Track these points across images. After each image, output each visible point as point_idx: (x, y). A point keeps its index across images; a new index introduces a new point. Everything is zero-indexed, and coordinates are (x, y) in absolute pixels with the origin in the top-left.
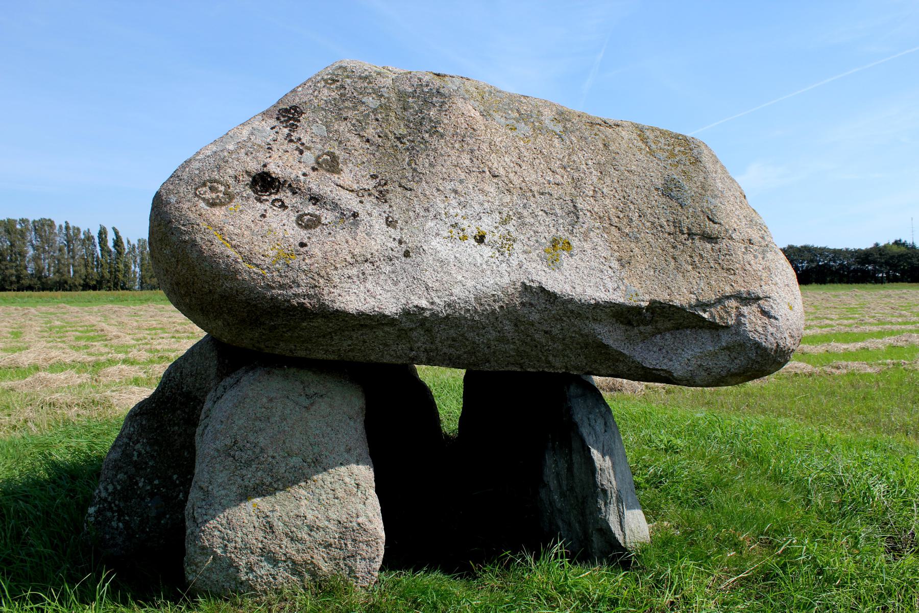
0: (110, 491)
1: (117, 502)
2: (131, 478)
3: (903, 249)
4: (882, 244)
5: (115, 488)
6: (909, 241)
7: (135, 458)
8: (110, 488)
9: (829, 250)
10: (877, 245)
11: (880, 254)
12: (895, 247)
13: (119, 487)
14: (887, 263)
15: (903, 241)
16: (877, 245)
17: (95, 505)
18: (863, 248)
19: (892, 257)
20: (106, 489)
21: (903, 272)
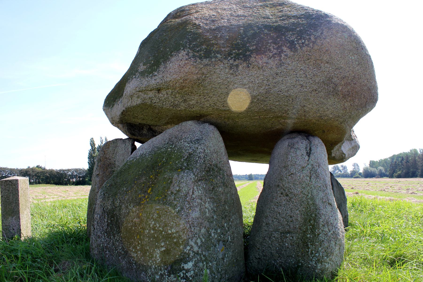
0: (199, 244)
1: (204, 253)
2: (208, 231)
3: (40, 170)
4: (31, 167)
5: (202, 241)
6: (43, 166)
7: (207, 215)
8: (199, 241)
9: (8, 169)
10: (29, 167)
11: (33, 171)
12: (37, 168)
13: (203, 240)
14: (36, 175)
15: (40, 166)
16: (29, 167)
17: (191, 260)
18: (48, 167)
19: (38, 173)
20: (196, 243)
21: (43, 180)
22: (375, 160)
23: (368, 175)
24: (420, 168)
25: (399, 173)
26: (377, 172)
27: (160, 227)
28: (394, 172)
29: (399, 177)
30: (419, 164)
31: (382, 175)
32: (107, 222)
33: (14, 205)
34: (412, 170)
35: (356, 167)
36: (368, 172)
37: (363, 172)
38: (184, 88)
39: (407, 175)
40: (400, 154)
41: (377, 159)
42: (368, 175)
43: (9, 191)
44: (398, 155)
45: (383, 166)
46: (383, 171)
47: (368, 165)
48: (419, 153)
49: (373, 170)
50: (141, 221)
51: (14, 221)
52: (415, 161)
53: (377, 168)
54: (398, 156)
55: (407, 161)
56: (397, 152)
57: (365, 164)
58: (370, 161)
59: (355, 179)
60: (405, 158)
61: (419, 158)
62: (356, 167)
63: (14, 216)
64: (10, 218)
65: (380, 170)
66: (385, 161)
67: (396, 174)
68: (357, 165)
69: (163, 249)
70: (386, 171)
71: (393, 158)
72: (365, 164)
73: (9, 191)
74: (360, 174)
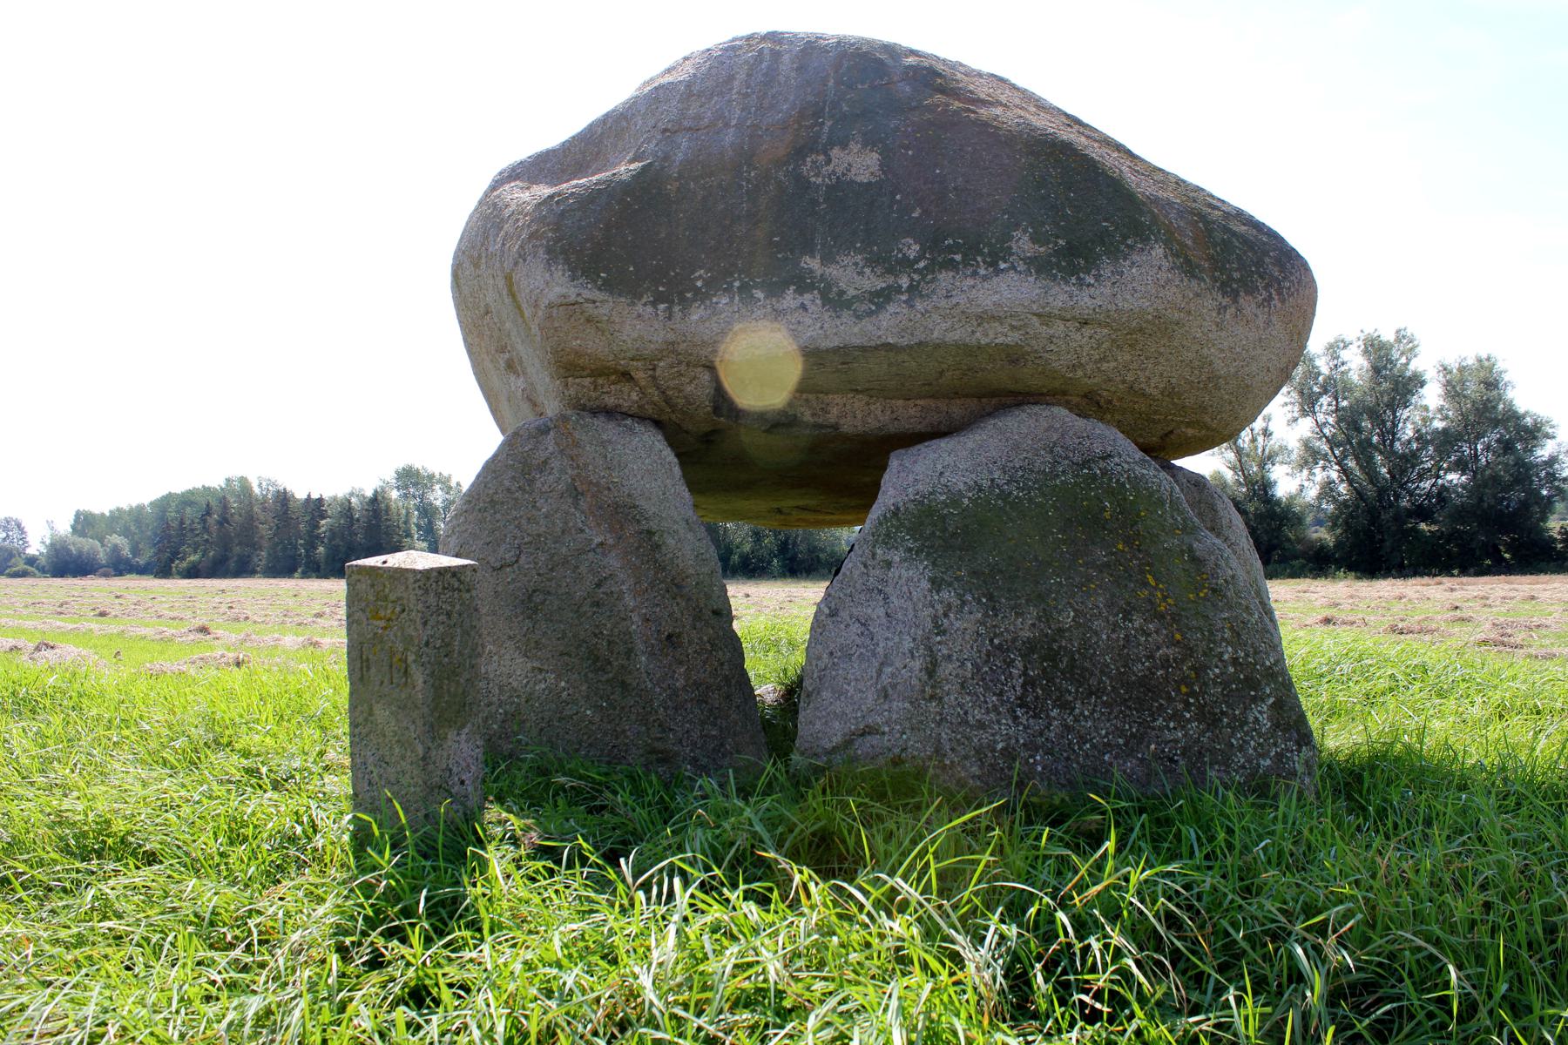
22: (96, 511)
23: (66, 563)
24: (265, 544)
25: (192, 558)
26: (102, 557)
27: (1247, 655)
28: (175, 555)
29: (193, 573)
30: (265, 530)
31: (120, 567)
32: (1025, 674)
33: (466, 675)
34: (237, 550)
35: (14, 534)
36: (68, 552)
37: (48, 556)
38: (1139, 333)
39: (217, 568)
40: (191, 492)
41: (102, 505)
42: (66, 563)
43: (449, 615)
44: (183, 494)
45: (126, 533)
46: (126, 552)
47: (64, 527)
48: (257, 490)
49: (87, 544)
50: (1190, 651)
51: (464, 746)
52: (251, 518)
53: (101, 541)
54: (187, 499)
55: (224, 521)
56: (180, 484)
57: (50, 524)
58: (78, 514)
59: (9, 581)
60: (214, 503)
61: (264, 509)
62: (14, 534)
63: (463, 726)
64: (451, 735)
65: (116, 549)
66: (137, 514)
67: (184, 565)
68: (19, 525)
69: (1272, 700)
70: (136, 551)
71: (164, 504)
72: (50, 524)
73: (449, 615)
74: (31, 561)
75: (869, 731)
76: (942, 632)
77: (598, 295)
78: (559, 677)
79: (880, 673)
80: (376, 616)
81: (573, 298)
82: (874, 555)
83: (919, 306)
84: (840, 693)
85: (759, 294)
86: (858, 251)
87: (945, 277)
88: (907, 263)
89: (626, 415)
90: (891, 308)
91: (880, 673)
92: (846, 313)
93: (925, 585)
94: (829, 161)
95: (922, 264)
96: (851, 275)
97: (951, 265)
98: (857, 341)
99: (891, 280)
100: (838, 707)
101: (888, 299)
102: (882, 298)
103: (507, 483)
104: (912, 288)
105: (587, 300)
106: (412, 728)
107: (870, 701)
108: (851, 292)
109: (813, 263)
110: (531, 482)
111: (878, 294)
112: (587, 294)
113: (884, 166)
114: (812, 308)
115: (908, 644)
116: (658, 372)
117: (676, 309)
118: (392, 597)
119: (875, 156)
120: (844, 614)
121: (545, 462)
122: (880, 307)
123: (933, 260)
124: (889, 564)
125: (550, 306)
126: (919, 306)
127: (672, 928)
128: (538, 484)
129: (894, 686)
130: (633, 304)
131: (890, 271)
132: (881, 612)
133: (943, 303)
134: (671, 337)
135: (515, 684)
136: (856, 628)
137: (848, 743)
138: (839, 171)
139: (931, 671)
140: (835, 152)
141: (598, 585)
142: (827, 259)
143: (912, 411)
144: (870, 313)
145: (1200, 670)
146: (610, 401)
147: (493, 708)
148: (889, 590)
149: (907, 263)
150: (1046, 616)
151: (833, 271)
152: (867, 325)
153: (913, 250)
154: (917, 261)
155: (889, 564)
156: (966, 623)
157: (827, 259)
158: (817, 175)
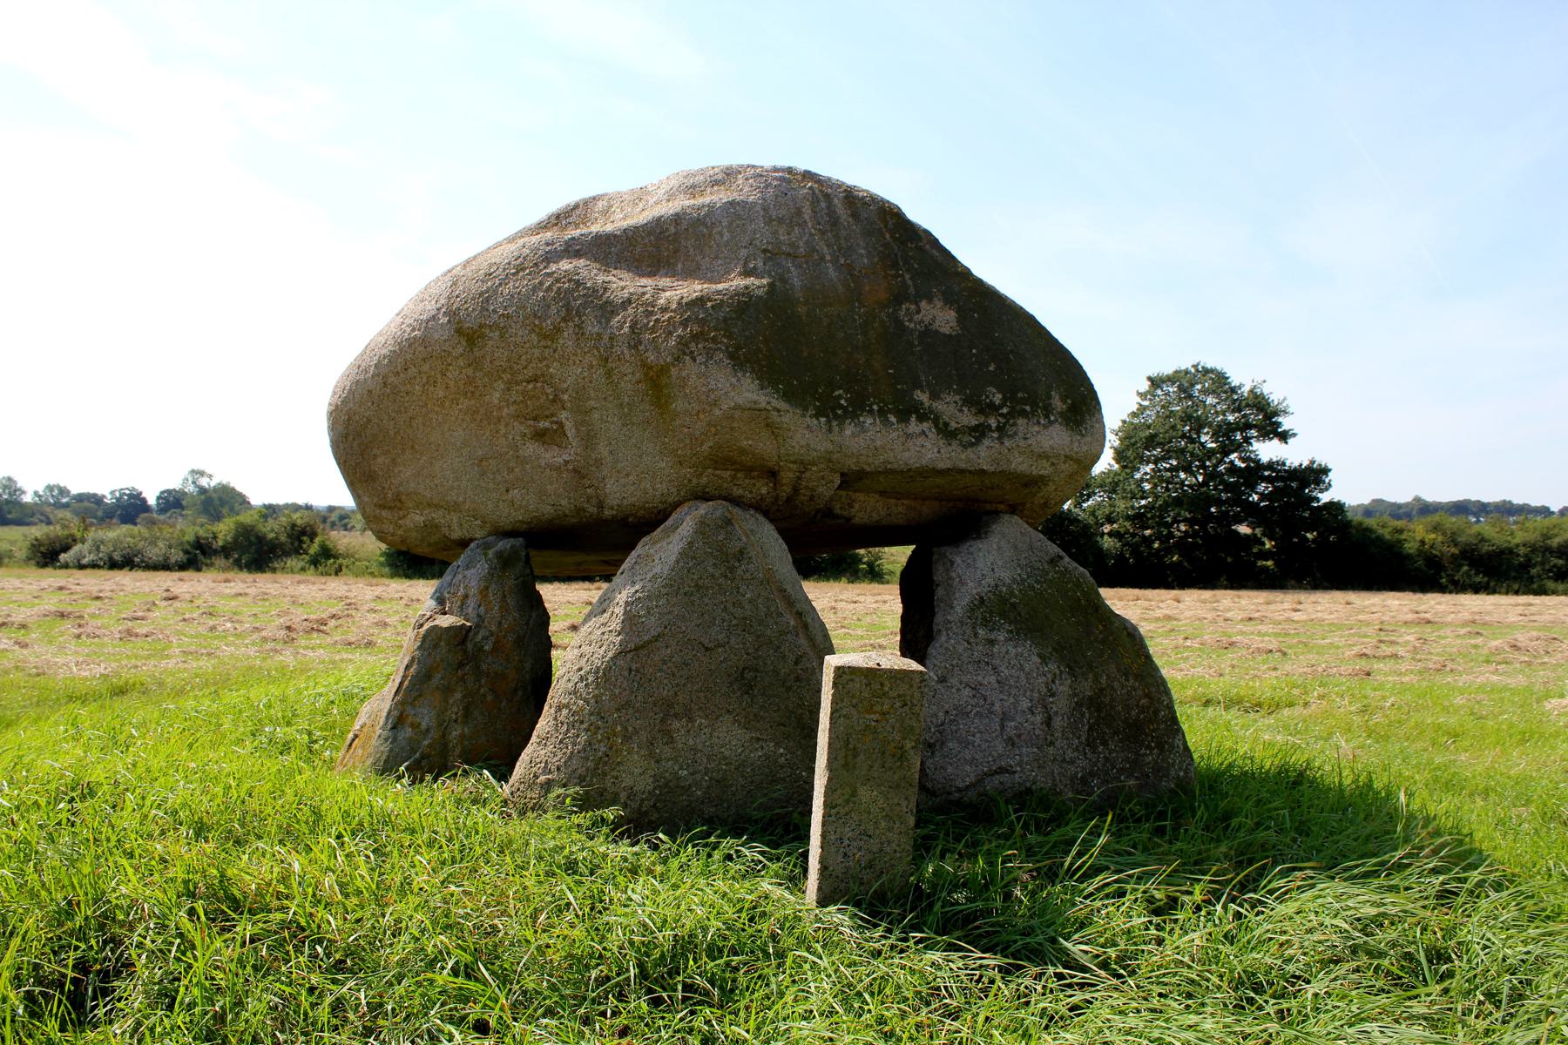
75: (1001, 770)
76: (1053, 695)
77: (782, 405)
78: (778, 745)
79: (1003, 727)
80: (870, 710)
81: (763, 405)
82: (976, 635)
83: (1007, 443)
84: (966, 744)
85: (893, 419)
86: (957, 392)
87: (1021, 421)
88: (993, 408)
89: (751, 506)
90: (986, 442)
91: (1003, 727)
92: (955, 443)
93: (1036, 659)
94: (918, 312)
95: (1005, 410)
96: (950, 408)
97: (1023, 414)
98: (963, 465)
99: (982, 419)
100: (967, 754)
101: (983, 435)
102: (980, 432)
103: (710, 570)
104: (1000, 429)
105: (775, 409)
106: (904, 804)
107: (1000, 749)
108: (953, 425)
109: (922, 397)
110: (732, 569)
111: (975, 429)
112: (775, 403)
113: (961, 320)
114: (930, 435)
115: (1025, 704)
116: (807, 474)
117: (834, 423)
118: (893, 694)
119: (953, 313)
120: (954, 681)
121: (741, 552)
122: (978, 441)
123: (1012, 408)
124: (992, 642)
125: (737, 407)
126: (1007, 443)
127: (1346, 926)
128: (739, 571)
129: (1019, 736)
130: (804, 416)
131: (981, 412)
132: (993, 679)
133: (1022, 443)
134: (830, 447)
135: (727, 753)
136: (967, 692)
137: (980, 781)
138: (927, 320)
139: (1048, 722)
140: (923, 304)
141: (796, 663)
142: (934, 396)
143: (900, 509)
144: (972, 445)
145: (1156, 712)
146: (737, 492)
147: (698, 777)
148: (997, 662)
149: (993, 408)
150: (1096, 679)
151: (939, 406)
152: (970, 453)
153: (997, 399)
154: (1001, 407)
155: (992, 642)
156: (1063, 688)
157: (934, 396)
158: (910, 321)
